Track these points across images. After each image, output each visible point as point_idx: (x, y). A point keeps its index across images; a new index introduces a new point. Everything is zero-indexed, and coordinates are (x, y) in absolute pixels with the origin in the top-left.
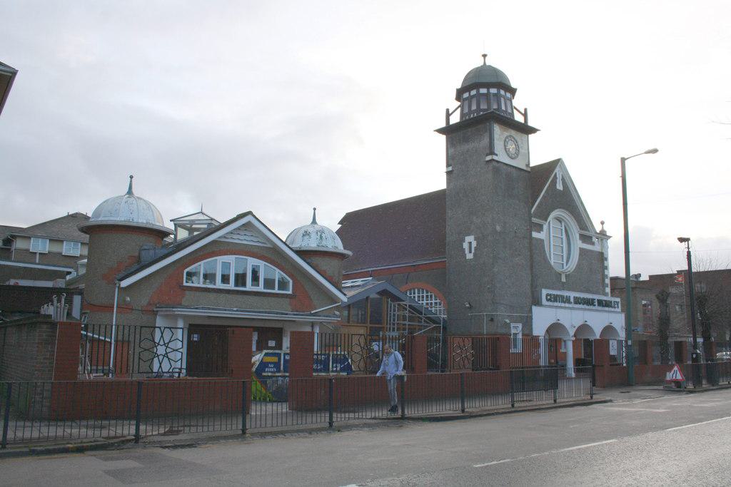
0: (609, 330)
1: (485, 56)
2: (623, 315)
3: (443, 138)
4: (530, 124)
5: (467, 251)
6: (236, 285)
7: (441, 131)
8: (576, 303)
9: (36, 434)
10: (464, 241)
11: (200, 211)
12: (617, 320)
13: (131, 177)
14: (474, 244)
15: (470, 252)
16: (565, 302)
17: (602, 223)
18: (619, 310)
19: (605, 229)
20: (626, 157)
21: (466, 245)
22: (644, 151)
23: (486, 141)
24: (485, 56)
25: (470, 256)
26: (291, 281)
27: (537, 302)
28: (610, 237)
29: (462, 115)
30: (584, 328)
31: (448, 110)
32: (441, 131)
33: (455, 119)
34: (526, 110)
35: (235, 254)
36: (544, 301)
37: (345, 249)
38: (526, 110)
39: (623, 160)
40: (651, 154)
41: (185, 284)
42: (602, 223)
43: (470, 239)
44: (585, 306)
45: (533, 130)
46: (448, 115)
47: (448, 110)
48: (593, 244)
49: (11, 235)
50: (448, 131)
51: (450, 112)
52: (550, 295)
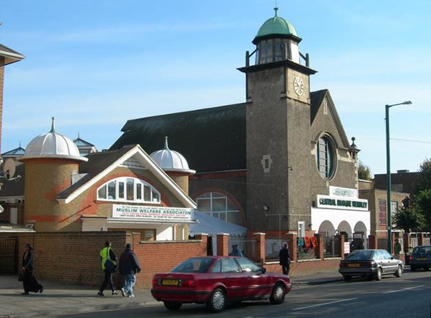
0: (360, 225)
1: (276, 9)
2: (369, 213)
3: (244, 74)
4: (311, 67)
5: (264, 167)
6: (128, 199)
7: (242, 70)
8: (354, 206)
9: (168, 284)
10: (262, 158)
11: (77, 138)
12: (364, 216)
13: (53, 119)
14: (271, 161)
15: (267, 167)
16: (331, 204)
17: (353, 139)
18: (367, 209)
19: (355, 144)
20: (389, 105)
21: (263, 162)
22: (404, 101)
23: (281, 83)
24: (276, 9)
25: (266, 171)
26: (160, 194)
27: (314, 205)
28: (359, 150)
29: (260, 58)
30: (344, 224)
31: (247, 52)
32: (242, 70)
33: (252, 62)
34: (307, 55)
35: (126, 176)
36: (319, 205)
37: (360, 197)
38: (307, 55)
39: (387, 107)
40: (406, 105)
41: (98, 199)
42: (353, 139)
43: (265, 157)
44: (344, 207)
45: (313, 72)
46: (248, 56)
47: (247, 52)
48: (347, 156)
49: (34, 174)
50: (246, 70)
51: (250, 54)
52: (322, 200)
